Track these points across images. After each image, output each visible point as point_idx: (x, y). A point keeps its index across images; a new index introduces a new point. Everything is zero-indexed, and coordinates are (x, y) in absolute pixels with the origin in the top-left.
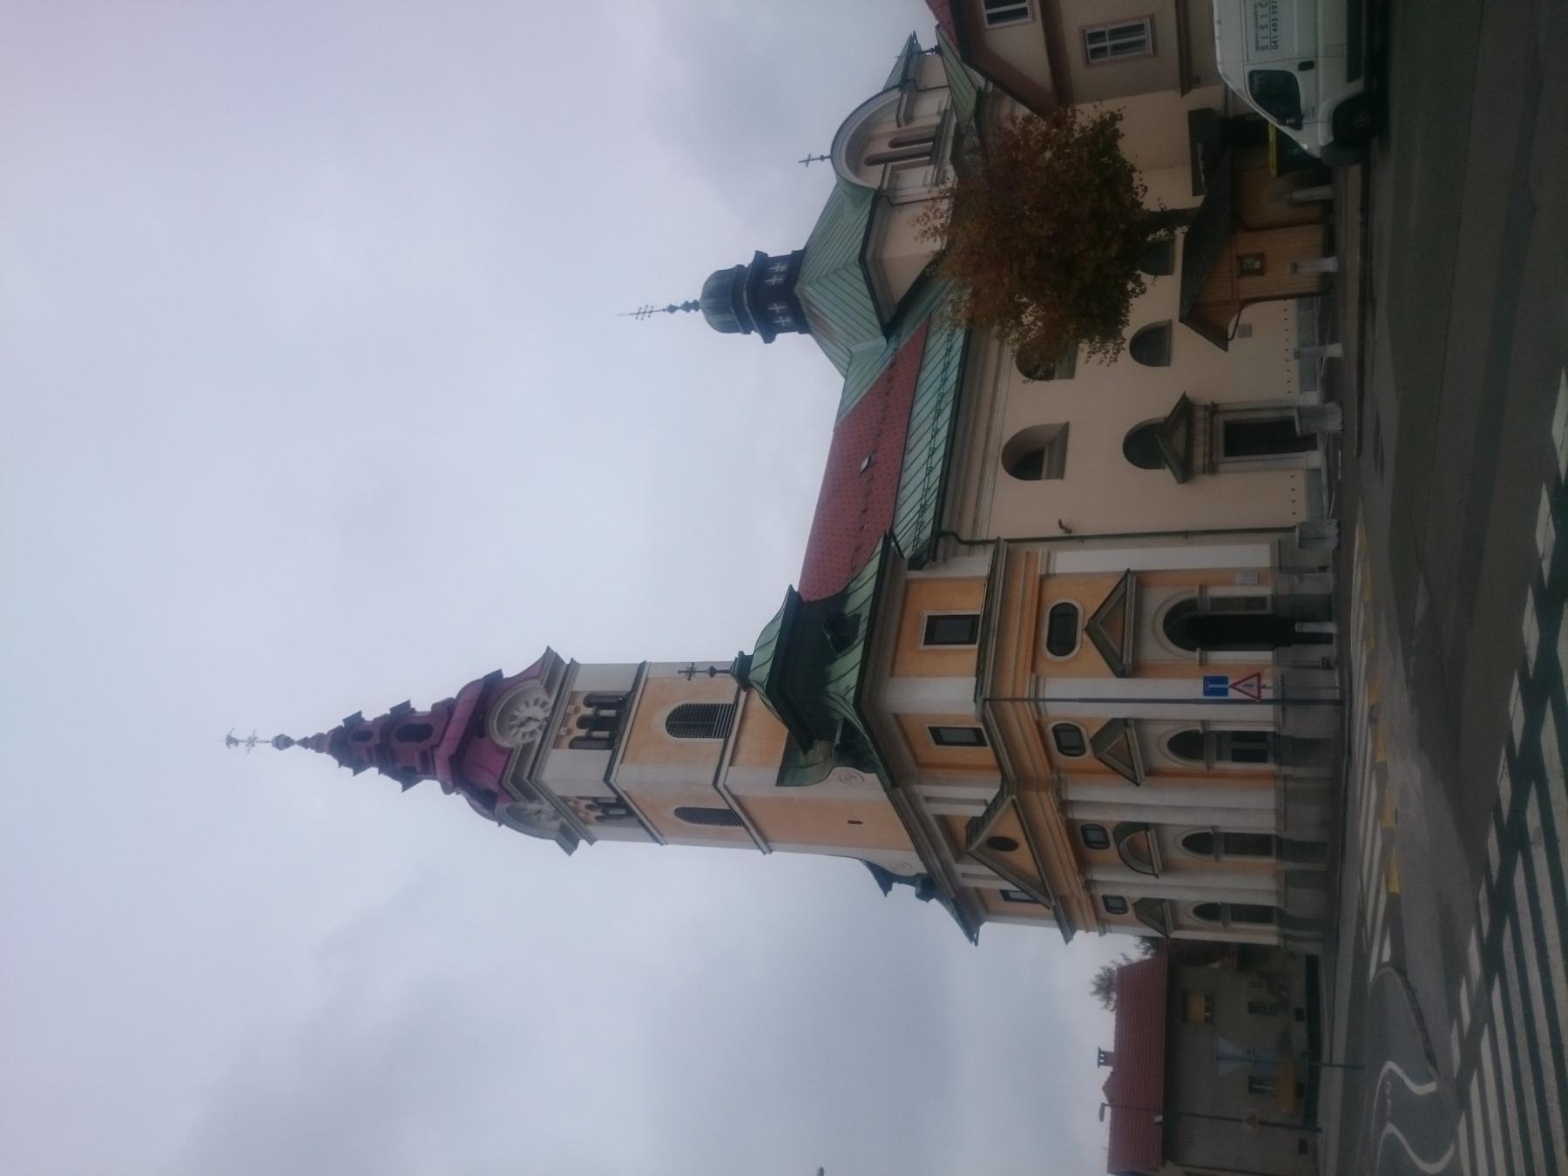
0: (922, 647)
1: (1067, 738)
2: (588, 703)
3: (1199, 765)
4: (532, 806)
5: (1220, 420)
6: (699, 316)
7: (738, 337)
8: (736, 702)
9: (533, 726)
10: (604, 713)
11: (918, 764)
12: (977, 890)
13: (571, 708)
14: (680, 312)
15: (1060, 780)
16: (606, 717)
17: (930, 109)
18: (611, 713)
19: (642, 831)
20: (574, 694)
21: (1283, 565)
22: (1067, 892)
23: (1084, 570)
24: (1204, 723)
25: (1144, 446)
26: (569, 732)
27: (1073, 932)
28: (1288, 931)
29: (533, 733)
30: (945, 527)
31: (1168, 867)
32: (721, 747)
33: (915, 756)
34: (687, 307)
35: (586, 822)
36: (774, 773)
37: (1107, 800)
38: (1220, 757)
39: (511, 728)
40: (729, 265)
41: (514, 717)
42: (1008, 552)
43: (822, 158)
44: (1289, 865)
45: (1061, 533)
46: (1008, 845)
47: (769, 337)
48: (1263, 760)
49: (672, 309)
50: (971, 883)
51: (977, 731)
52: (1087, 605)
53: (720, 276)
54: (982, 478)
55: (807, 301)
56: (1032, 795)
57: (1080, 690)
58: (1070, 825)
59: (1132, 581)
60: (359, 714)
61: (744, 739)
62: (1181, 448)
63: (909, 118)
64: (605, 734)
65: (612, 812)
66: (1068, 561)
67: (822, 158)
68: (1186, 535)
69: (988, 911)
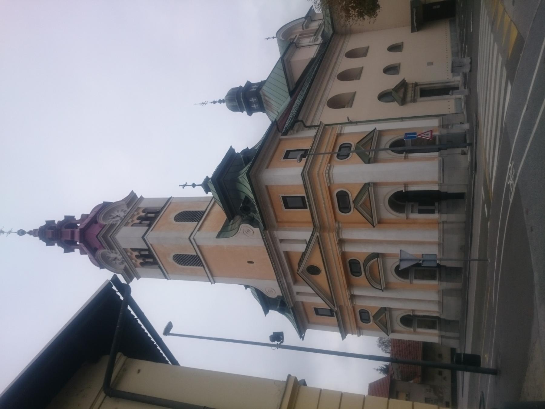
0: (282, 160)
1: (343, 201)
2: (143, 211)
3: (403, 216)
4: (113, 255)
5: (418, 88)
6: (224, 105)
7: (239, 114)
8: (206, 210)
9: (118, 218)
10: (149, 215)
11: (277, 221)
12: (302, 302)
13: (136, 213)
14: (217, 104)
15: (339, 228)
16: (148, 215)
17: (315, 25)
18: (153, 215)
19: (159, 270)
20: (139, 208)
21: (444, 126)
22: (343, 304)
23: (353, 133)
24: (413, 311)
25: (384, 96)
26: (132, 221)
27: (346, 335)
28: (443, 333)
29: (117, 221)
30: (300, 118)
31: (387, 287)
32: (195, 225)
33: (276, 217)
34: (220, 101)
35: (136, 266)
36: (216, 233)
37: (362, 239)
38: (412, 212)
39: (108, 219)
40: (237, 86)
41: (111, 216)
42: (324, 129)
43: (273, 38)
44: (445, 285)
45: (347, 121)
46: (314, 270)
47: (250, 114)
48: (432, 212)
49: (214, 102)
50: (300, 299)
51: (303, 198)
52: (353, 142)
53: (233, 89)
54: (317, 108)
55: (265, 95)
56: (326, 235)
57: (351, 174)
58: (344, 255)
59: (376, 134)
60: (65, 252)
61: (206, 223)
62: (402, 95)
63: (307, 27)
64: (148, 222)
65: (147, 260)
66: (348, 129)
67: (273, 38)
68: (402, 119)
69: (309, 322)
